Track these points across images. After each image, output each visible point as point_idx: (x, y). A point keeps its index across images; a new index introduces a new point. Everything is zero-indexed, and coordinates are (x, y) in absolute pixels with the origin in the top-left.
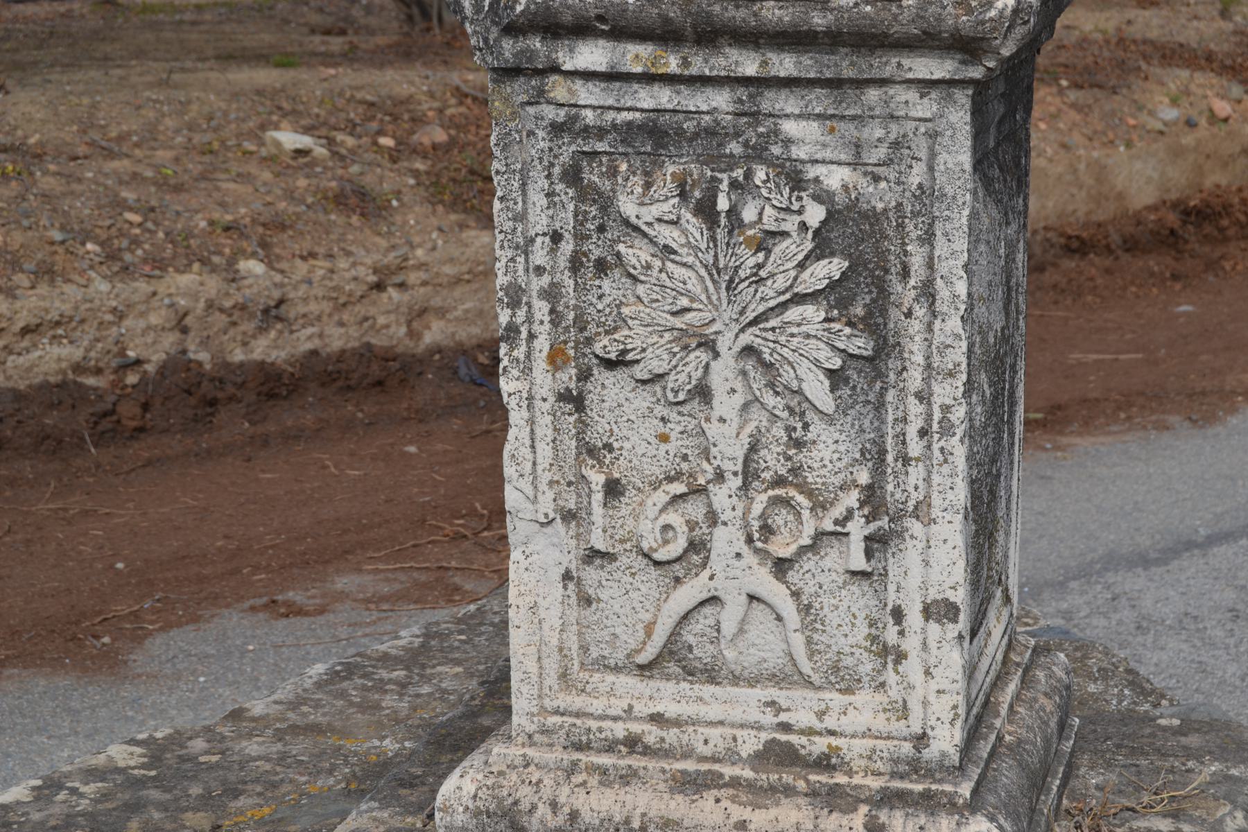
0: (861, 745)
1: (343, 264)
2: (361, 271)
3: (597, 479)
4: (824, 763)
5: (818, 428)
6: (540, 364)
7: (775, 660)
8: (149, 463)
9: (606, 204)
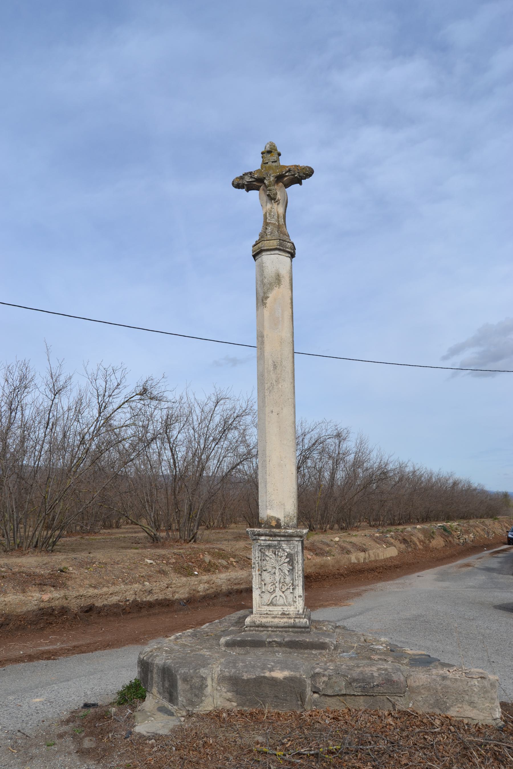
0: (292, 612)
1: (162, 583)
2: (165, 584)
3: (263, 583)
4: (288, 614)
5: (287, 577)
6: (257, 571)
7: (283, 603)
8: (132, 618)
9: (264, 553)
